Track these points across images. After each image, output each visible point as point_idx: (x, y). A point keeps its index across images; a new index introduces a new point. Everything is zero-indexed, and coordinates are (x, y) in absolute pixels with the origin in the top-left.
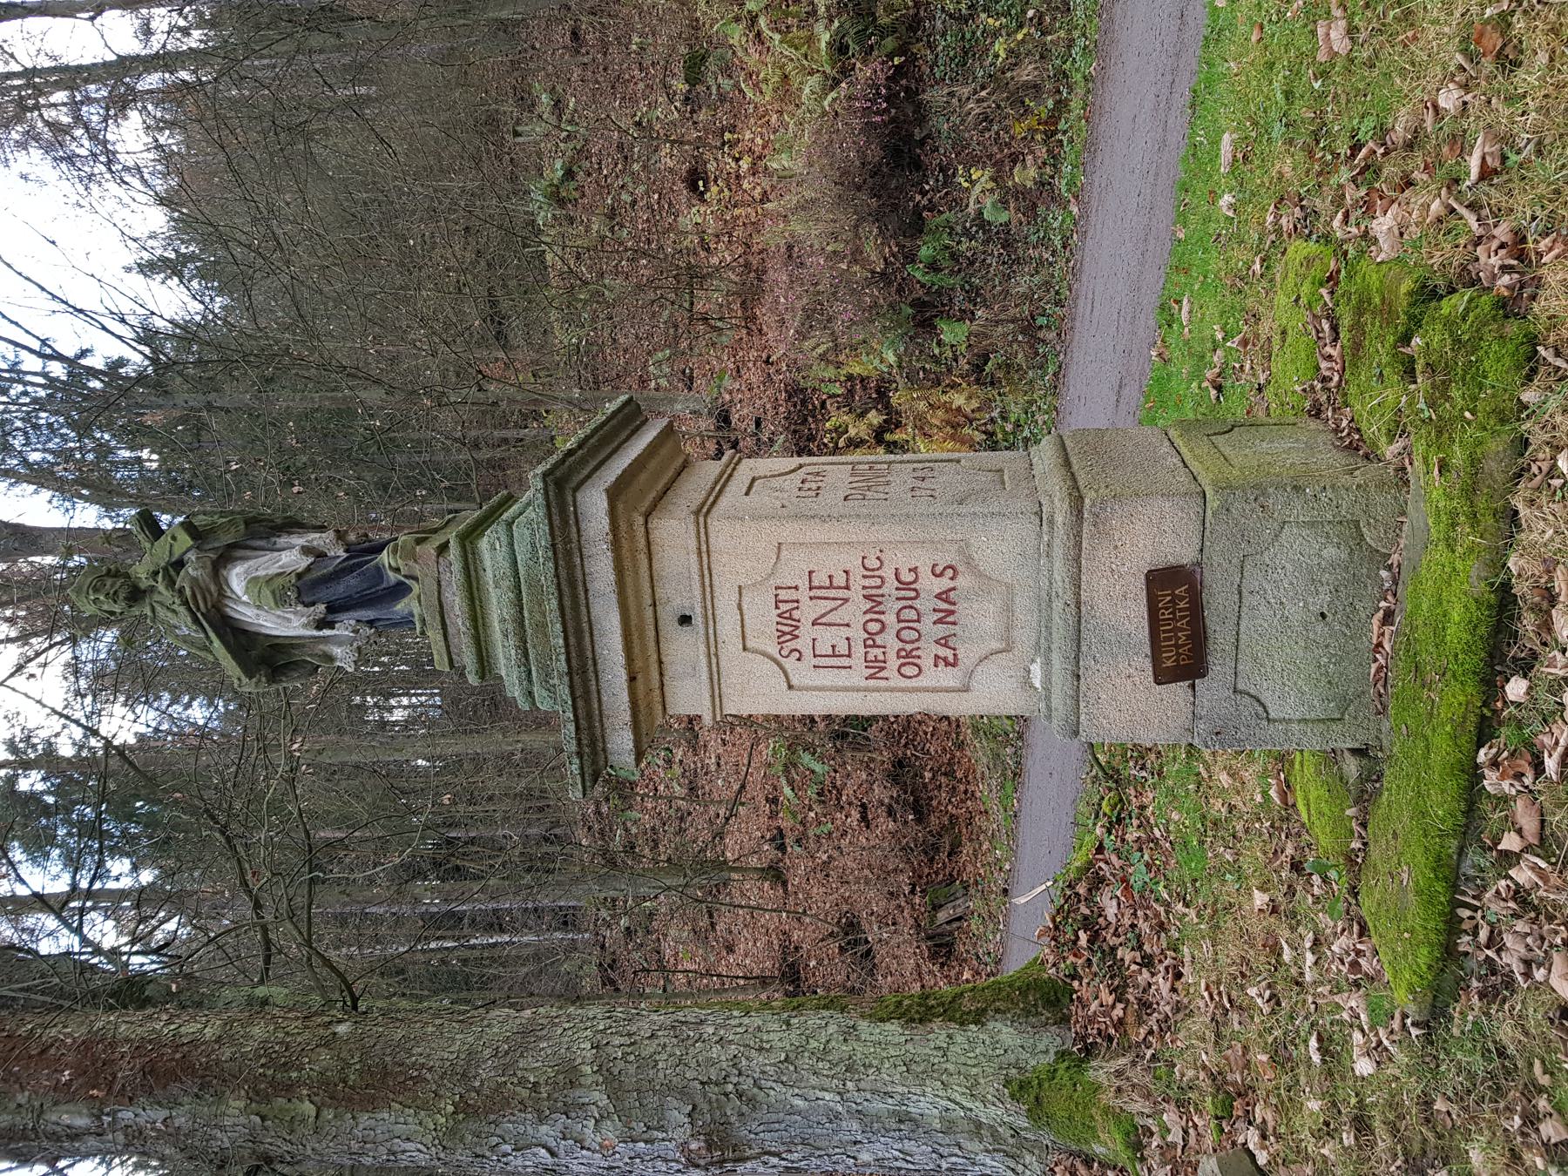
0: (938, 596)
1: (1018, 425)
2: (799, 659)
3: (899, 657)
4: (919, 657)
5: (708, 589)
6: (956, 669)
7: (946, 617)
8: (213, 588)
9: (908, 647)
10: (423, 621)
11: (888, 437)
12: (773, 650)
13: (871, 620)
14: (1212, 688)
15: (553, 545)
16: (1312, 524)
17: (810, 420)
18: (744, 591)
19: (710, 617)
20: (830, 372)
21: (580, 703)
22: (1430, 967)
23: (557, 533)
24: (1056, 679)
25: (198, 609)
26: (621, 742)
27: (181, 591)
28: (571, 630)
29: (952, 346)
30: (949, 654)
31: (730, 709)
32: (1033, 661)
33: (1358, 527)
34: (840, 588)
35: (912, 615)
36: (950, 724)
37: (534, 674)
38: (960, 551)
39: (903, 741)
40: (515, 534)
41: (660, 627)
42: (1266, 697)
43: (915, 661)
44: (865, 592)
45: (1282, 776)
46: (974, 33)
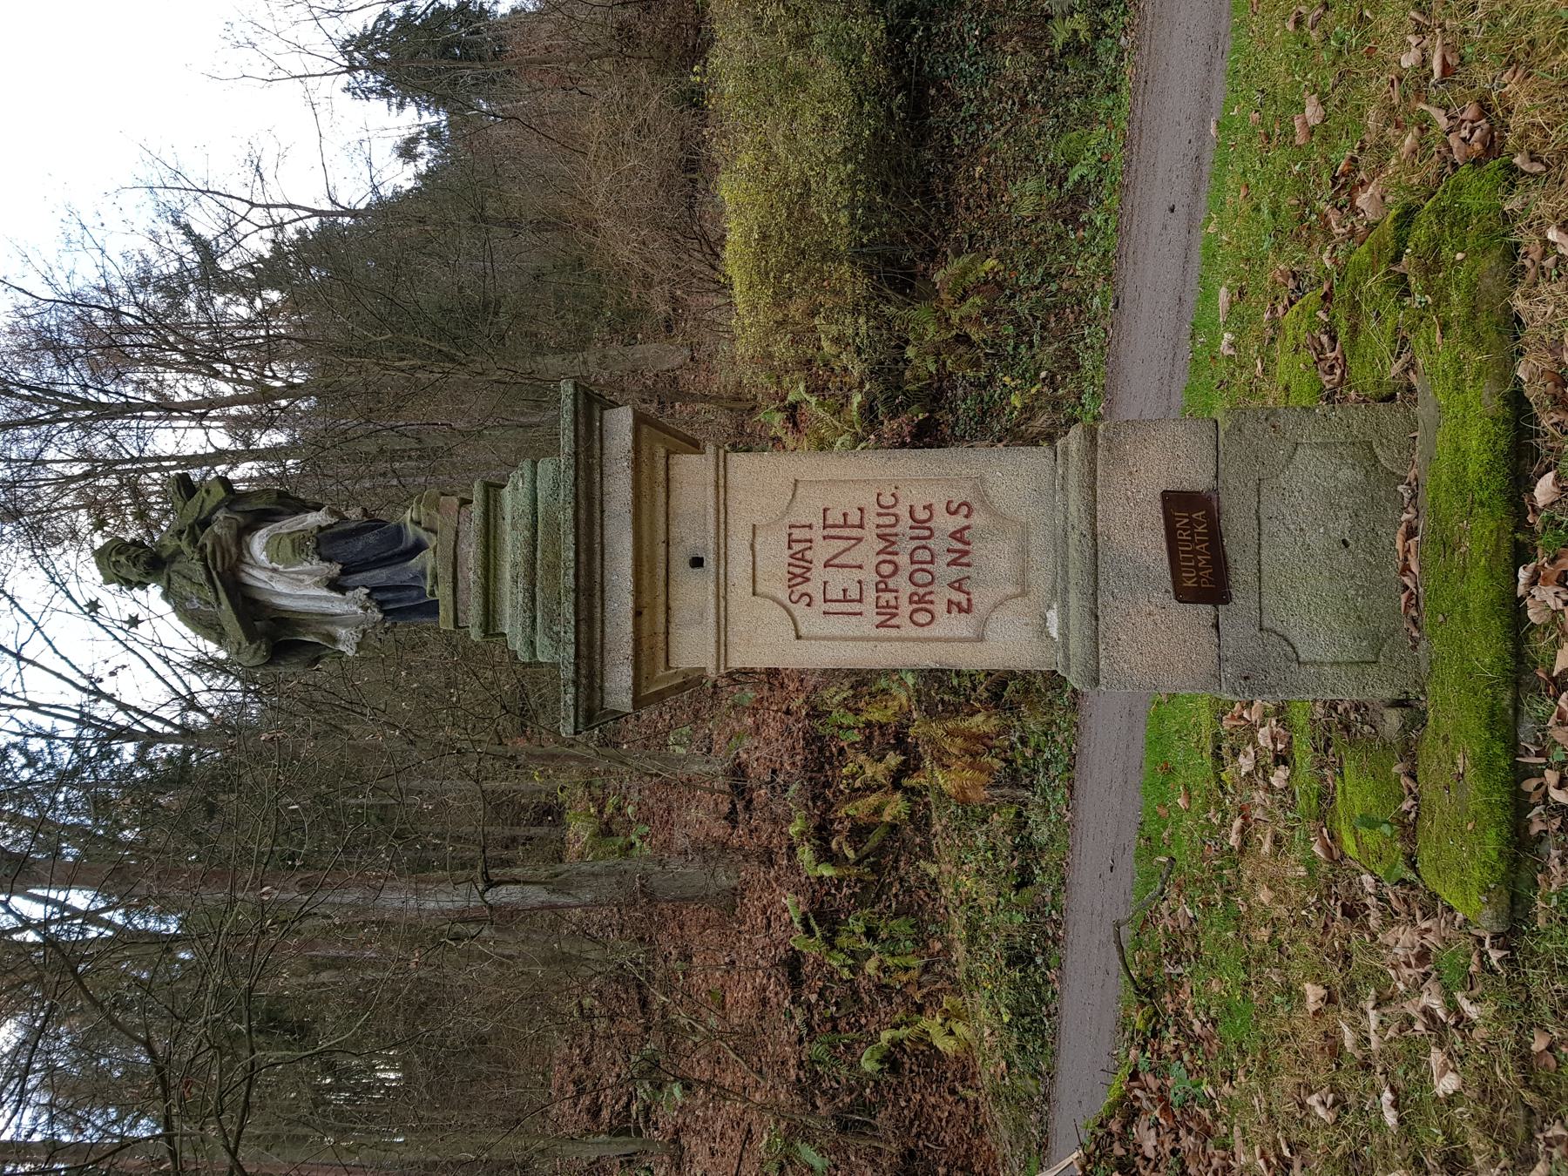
0: (953, 536)
1: (1038, 751)
2: (809, 605)
3: (911, 602)
4: (932, 602)
5: (722, 526)
6: (969, 616)
7: (960, 558)
8: (233, 550)
9: (921, 591)
10: (435, 577)
11: (906, 782)
12: (783, 596)
13: (884, 562)
14: (1238, 613)
15: (576, 454)
16: (1325, 446)
17: (827, 767)
18: (758, 531)
19: (723, 556)
20: (849, 720)
21: (583, 628)
22: (1500, 853)
23: (581, 442)
24: (1074, 622)
25: (215, 568)
26: (619, 683)
27: (202, 548)
28: (583, 546)
29: (971, 675)
30: (962, 598)
31: (736, 662)
32: (1049, 607)
33: (1371, 449)
34: (853, 601)
35: (926, 556)
36: (967, 1106)
37: (539, 620)
38: (975, 488)
39: (914, 1131)
40: (539, 470)
41: (672, 569)
42: (1295, 635)
43: (928, 606)
44: (879, 531)
45: (1325, 830)
46: (991, 397)
